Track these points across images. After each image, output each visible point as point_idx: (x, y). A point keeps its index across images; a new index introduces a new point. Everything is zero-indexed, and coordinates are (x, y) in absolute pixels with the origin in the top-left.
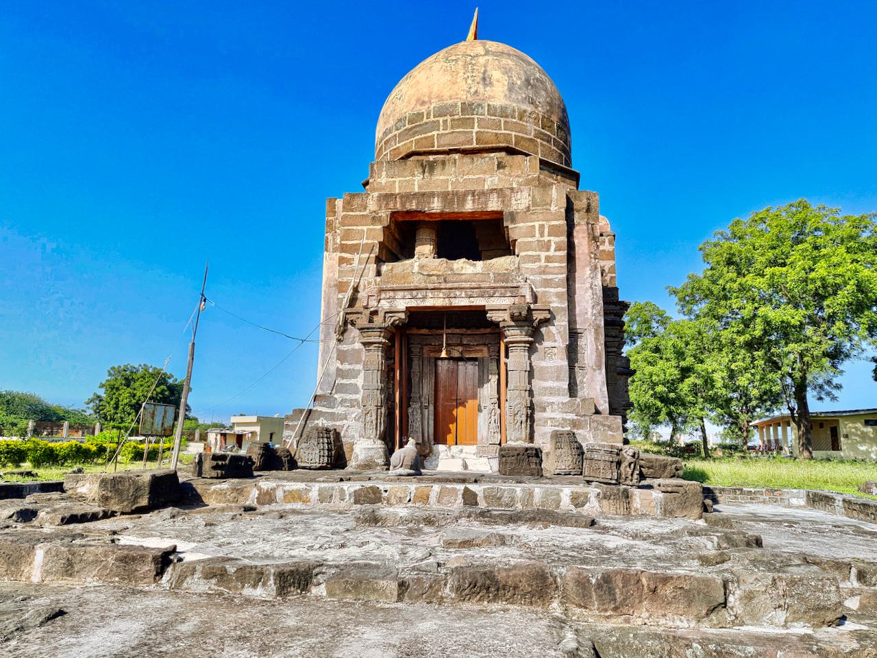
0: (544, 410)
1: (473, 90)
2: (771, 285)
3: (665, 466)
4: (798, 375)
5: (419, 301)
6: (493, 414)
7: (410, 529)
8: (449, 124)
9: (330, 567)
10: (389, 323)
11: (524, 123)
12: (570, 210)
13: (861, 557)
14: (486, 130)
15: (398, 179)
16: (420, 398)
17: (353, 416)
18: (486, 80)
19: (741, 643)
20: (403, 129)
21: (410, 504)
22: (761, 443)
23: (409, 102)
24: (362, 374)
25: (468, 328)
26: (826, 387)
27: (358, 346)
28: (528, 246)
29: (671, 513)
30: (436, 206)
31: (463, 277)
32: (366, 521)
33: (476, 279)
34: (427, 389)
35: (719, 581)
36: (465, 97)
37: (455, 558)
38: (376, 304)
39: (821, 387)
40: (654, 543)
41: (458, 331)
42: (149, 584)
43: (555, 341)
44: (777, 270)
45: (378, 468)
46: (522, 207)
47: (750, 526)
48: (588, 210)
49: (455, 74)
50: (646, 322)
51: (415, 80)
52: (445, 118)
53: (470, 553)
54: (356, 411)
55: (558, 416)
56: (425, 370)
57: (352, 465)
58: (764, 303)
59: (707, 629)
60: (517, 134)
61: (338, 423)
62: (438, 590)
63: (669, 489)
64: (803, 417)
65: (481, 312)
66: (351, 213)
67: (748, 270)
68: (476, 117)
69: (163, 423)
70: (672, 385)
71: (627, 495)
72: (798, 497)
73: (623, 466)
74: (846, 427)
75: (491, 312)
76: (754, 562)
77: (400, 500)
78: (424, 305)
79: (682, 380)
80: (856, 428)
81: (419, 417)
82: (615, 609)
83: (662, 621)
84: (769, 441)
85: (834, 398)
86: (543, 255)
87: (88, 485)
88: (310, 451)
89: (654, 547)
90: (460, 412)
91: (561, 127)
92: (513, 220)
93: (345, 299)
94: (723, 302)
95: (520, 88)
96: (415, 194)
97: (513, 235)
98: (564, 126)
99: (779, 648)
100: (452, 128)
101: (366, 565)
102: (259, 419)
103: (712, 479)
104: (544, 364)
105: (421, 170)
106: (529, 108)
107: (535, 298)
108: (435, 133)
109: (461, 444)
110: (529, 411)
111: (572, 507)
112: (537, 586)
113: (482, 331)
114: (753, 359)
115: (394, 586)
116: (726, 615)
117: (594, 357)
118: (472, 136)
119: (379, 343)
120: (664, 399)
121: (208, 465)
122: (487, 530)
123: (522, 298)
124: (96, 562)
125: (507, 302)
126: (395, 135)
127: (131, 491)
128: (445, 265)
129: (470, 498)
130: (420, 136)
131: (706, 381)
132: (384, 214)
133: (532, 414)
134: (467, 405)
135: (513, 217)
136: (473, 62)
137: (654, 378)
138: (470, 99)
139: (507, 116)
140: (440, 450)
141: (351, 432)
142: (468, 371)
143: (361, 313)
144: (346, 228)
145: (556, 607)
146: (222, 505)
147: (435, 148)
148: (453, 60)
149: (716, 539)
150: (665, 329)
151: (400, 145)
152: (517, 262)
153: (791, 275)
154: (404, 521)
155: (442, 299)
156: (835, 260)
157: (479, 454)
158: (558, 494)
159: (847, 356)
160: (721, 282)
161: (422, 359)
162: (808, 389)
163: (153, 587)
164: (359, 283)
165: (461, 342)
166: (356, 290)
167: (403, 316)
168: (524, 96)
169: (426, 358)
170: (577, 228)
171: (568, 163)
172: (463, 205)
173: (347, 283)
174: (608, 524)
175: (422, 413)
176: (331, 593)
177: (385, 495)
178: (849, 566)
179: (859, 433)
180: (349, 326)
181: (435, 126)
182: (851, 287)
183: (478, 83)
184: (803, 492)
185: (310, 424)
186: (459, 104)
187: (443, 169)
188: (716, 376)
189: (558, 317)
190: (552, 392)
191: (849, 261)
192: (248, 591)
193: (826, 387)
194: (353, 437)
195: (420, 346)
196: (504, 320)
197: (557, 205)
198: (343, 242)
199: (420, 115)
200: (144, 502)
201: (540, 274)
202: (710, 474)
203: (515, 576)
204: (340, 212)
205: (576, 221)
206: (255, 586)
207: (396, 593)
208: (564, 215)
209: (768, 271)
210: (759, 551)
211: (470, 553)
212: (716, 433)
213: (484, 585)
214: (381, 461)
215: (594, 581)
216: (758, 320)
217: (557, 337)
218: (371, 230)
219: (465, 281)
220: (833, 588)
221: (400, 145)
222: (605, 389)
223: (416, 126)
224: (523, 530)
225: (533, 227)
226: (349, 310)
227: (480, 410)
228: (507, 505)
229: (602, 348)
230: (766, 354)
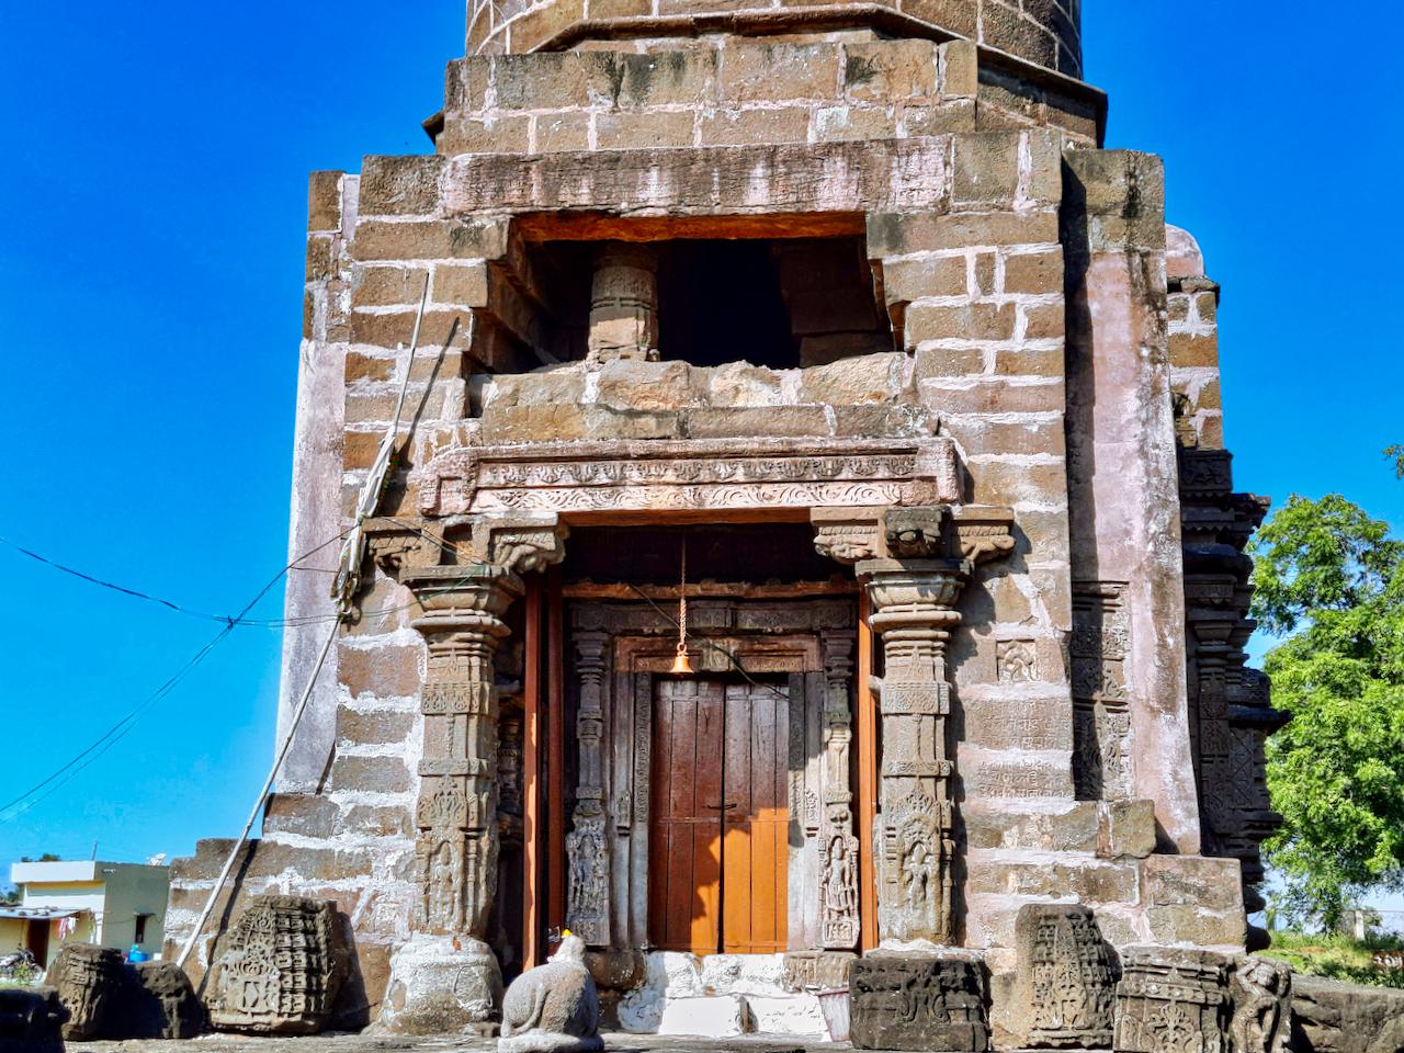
5: (600, 495)
6: (836, 851)
10: (505, 561)
12: (1073, 209)
15: (533, 114)
16: (603, 802)
17: (391, 860)
24: (419, 726)
25: (757, 580)
27: (405, 637)
28: (942, 323)
30: (654, 196)
31: (740, 420)
33: (780, 425)
34: (626, 772)
38: (463, 504)
43: (1030, 620)
45: (469, 1028)
46: (924, 199)
50: (1326, 559)
55: (1041, 857)
65: (795, 529)
66: (385, 219)
73: (1240, 1017)
75: (828, 530)
78: (616, 507)
86: (990, 349)
92: (896, 241)
93: (365, 493)
96: (588, 159)
97: (894, 289)
102: (101, 868)
104: (993, 693)
105: (606, 84)
107: (966, 484)
109: (736, 948)
110: (949, 845)
113: (801, 588)
117: (1152, 670)
123: (926, 485)
125: (879, 496)
132: (491, 222)
133: (959, 851)
134: (755, 826)
137: (1353, 735)
140: (668, 970)
141: (383, 914)
142: (757, 715)
143: (416, 533)
144: (369, 264)
147: (654, 16)
150: (1387, 581)
152: (908, 373)
155: (672, 489)
157: (795, 981)
161: (608, 675)
164: (411, 437)
165: (735, 622)
166: (400, 460)
167: (548, 541)
170: (1096, 268)
171: (1071, 61)
173: (373, 440)
175: (611, 851)
180: (379, 574)
185: (253, 889)
187: (678, 79)
189: (1038, 547)
190: (1026, 782)
194: (389, 930)
195: (605, 637)
196: (869, 556)
198: (362, 310)
201: (982, 408)
205: (1093, 243)
208: (1055, 224)
214: (476, 1006)
219: (748, 433)
225: (960, 262)
226: (380, 524)
227: (795, 840)
229: (1176, 641)
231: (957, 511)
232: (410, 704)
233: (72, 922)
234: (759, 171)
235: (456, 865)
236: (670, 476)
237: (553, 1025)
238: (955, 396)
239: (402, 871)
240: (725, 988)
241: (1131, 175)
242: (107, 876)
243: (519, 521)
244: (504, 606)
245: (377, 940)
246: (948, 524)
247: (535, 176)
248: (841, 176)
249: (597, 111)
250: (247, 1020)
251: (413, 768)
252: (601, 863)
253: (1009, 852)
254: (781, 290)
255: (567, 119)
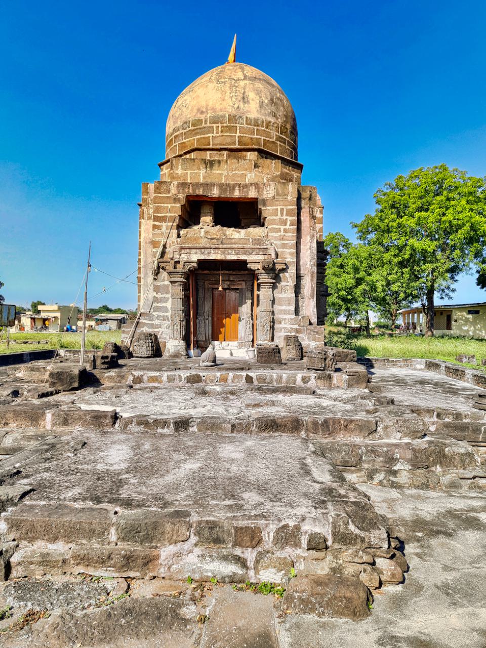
0: (280, 323)
1: (236, 106)
2: (418, 224)
3: (347, 355)
4: (430, 284)
7: (223, 397)
8: (220, 129)
9: (196, 418)
10: (187, 268)
11: (269, 131)
12: (299, 199)
13: (440, 406)
14: (245, 135)
15: (189, 172)
17: (165, 326)
18: (244, 99)
19: (381, 446)
20: (188, 129)
21: (218, 383)
22: (403, 325)
23: (192, 110)
24: (170, 300)
25: (233, 270)
26: (446, 290)
27: (167, 283)
28: (273, 222)
29: (351, 386)
30: (215, 193)
31: (233, 241)
32: (200, 394)
33: (241, 242)
34: (207, 307)
35: (374, 421)
36: (231, 111)
37: (255, 413)
38: (178, 257)
39: (443, 290)
40: (345, 403)
41: (227, 272)
42: (110, 428)
43: (288, 282)
44: (423, 214)
46: (270, 196)
47: (391, 389)
48: (310, 199)
49: (224, 93)
50: (336, 247)
51: (196, 94)
52: (217, 125)
53: (260, 410)
54: (167, 323)
55: (288, 326)
56: (206, 296)
57: (166, 355)
58: (413, 236)
59: (368, 441)
60: (265, 138)
61: (156, 330)
62: (250, 428)
63: (351, 374)
64: (430, 310)
65: (244, 263)
66: (159, 195)
67: (404, 213)
68: (238, 125)
69: (8, 318)
70: (350, 290)
71: (330, 377)
72: (421, 364)
73: (327, 360)
74: (456, 315)
76: (390, 412)
77: (212, 381)
79: (356, 286)
80: (462, 315)
81: (203, 325)
82: (329, 434)
83: (349, 439)
84: (408, 323)
85: (450, 298)
86: (282, 228)
87: (22, 372)
88: (141, 347)
89: (345, 406)
90: (227, 321)
91: (292, 131)
92: (264, 205)
93: (158, 253)
94: (386, 235)
95: (267, 105)
96: (202, 184)
97: (264, 214)
98: (294, 131)
99: (396, 448)
100: (222, 132)
101: (212, 417)
102: (59, 307)
103: (371, 352)
104: (281, 296)
105: (204, 166)
106: (273, 120)
107: (277, 256)
108: (211, 135)
109: (228, 340)
110: (272, 324)
111: (302, 383)
112: (294, 425)
113: (242, 272)
114: (402, 273)
115: (230, 426)
116: (376, 435)
117: (310, 291)
118: (234, 139)
119: (181, 282)
120: (344, 300)
121: (99, 362)
122: (262, 397)
124: (80, 418)
125: (260, 258)
126: (182, 133)
127: (68, 379)
128: (221, 232)
129: (249, 380)
130: (200, 136)
131: (372, 288)
132: (182, 196)
133: (273, 325)
135: (264, 202)
136: (236, 85)
137: (339, 286)
138: (234, 112)
139: (258, 126)
141: (164, 335)
142: (233, 296)
144: (157, 205)
145: (303, 434)
146: (112, 384)
147: (211, 147)
148: (222, 82)
149: (373, 401)
150: (348, 251)
151: (186, 140)
152: (266, 232)
153: (431, 218)
154: (219, 393)
156: (459, 209)
157: (240, 346)
158: (295, 377)
159: (461, 270)
160: (386, 221)
162: (435, 292)
163: (112, 430)
166: (165, 247)
167: (195, 265)
168: (269, 111)
169: (211, 292)
170: (303, 210)
171: (296, 158)
172: (233, 193)
173: (159, 242)
174: (321, 393)
176: (199, 430)
177: (204, 378)
178: (434, 411)
179: (464, 318)
180: (161, 270)
181: (210, 130)
182: (467, 228)
183: (240, 101)
184: (424, 361)
185: (139, 331)
186: (227, 115)
187: (219, 166)
188: (379, 285)
189: (290, 268)
190: (286, 312)
191: (468, 210)
192: (160, 430)
193: (446, 290)
194: (165, 338)
196: (258, 269)
197: (292, 197)
198: (155, 214)
199: (200, 121)
200: (76, 385)
201: (280, 240)
202: (370, 349)
203: (285, 421)
204: (152, 195)
205: (303, 205)
206: (163, 428)
207: (230, 430)
208: (296, 202)
209: (417, 215)
210: (392, 407)
211: (260, 410)
212: (374, 317)
213: (271, 425)
214: (184, 353)
215: (320, 423)
216: (408, 248)
217: (289, 280)
218: (173, 207)
219: (235, 243)
220: (422, 423)
221: (186, 140)
222: (315, 310)
223: (197, 129)
224: (280, 397)
225: (277, 209)
226: (161, 260)
227: (240, 320)
228: (269, 383)
229: (315, 285)
230: (411, 270)
231: (275, 261)
232: (169, 296)
233: (53, 319)
234: (237, 188)
235: (179, 327)
236: (220, 252)
237: (210, 362)
238: (275, 237)
239: (168, 328)
240: (226, 348)
241: (310, 191)
242: (60, 309)
243: (189, 260)
244: (186, 277)
245: (163, 340)
246: (274, 264)
247: (191, 187)
248: (254, 190)
249: (203, 172)
250: (140, 355)
251: (169, 309)
252: (203, 325)
253: (283, 325)
254: (239, 212)
255: (196, 173)
